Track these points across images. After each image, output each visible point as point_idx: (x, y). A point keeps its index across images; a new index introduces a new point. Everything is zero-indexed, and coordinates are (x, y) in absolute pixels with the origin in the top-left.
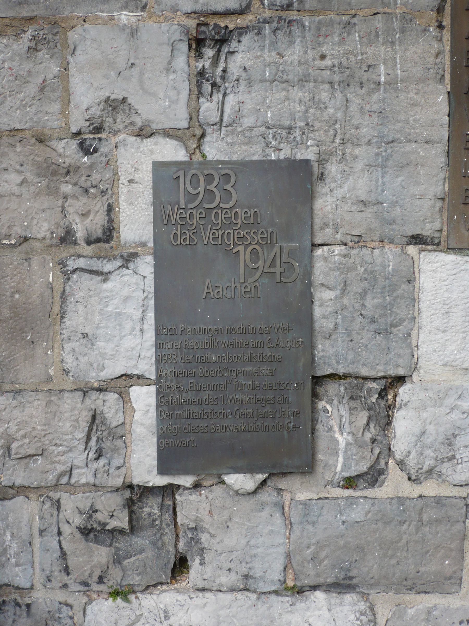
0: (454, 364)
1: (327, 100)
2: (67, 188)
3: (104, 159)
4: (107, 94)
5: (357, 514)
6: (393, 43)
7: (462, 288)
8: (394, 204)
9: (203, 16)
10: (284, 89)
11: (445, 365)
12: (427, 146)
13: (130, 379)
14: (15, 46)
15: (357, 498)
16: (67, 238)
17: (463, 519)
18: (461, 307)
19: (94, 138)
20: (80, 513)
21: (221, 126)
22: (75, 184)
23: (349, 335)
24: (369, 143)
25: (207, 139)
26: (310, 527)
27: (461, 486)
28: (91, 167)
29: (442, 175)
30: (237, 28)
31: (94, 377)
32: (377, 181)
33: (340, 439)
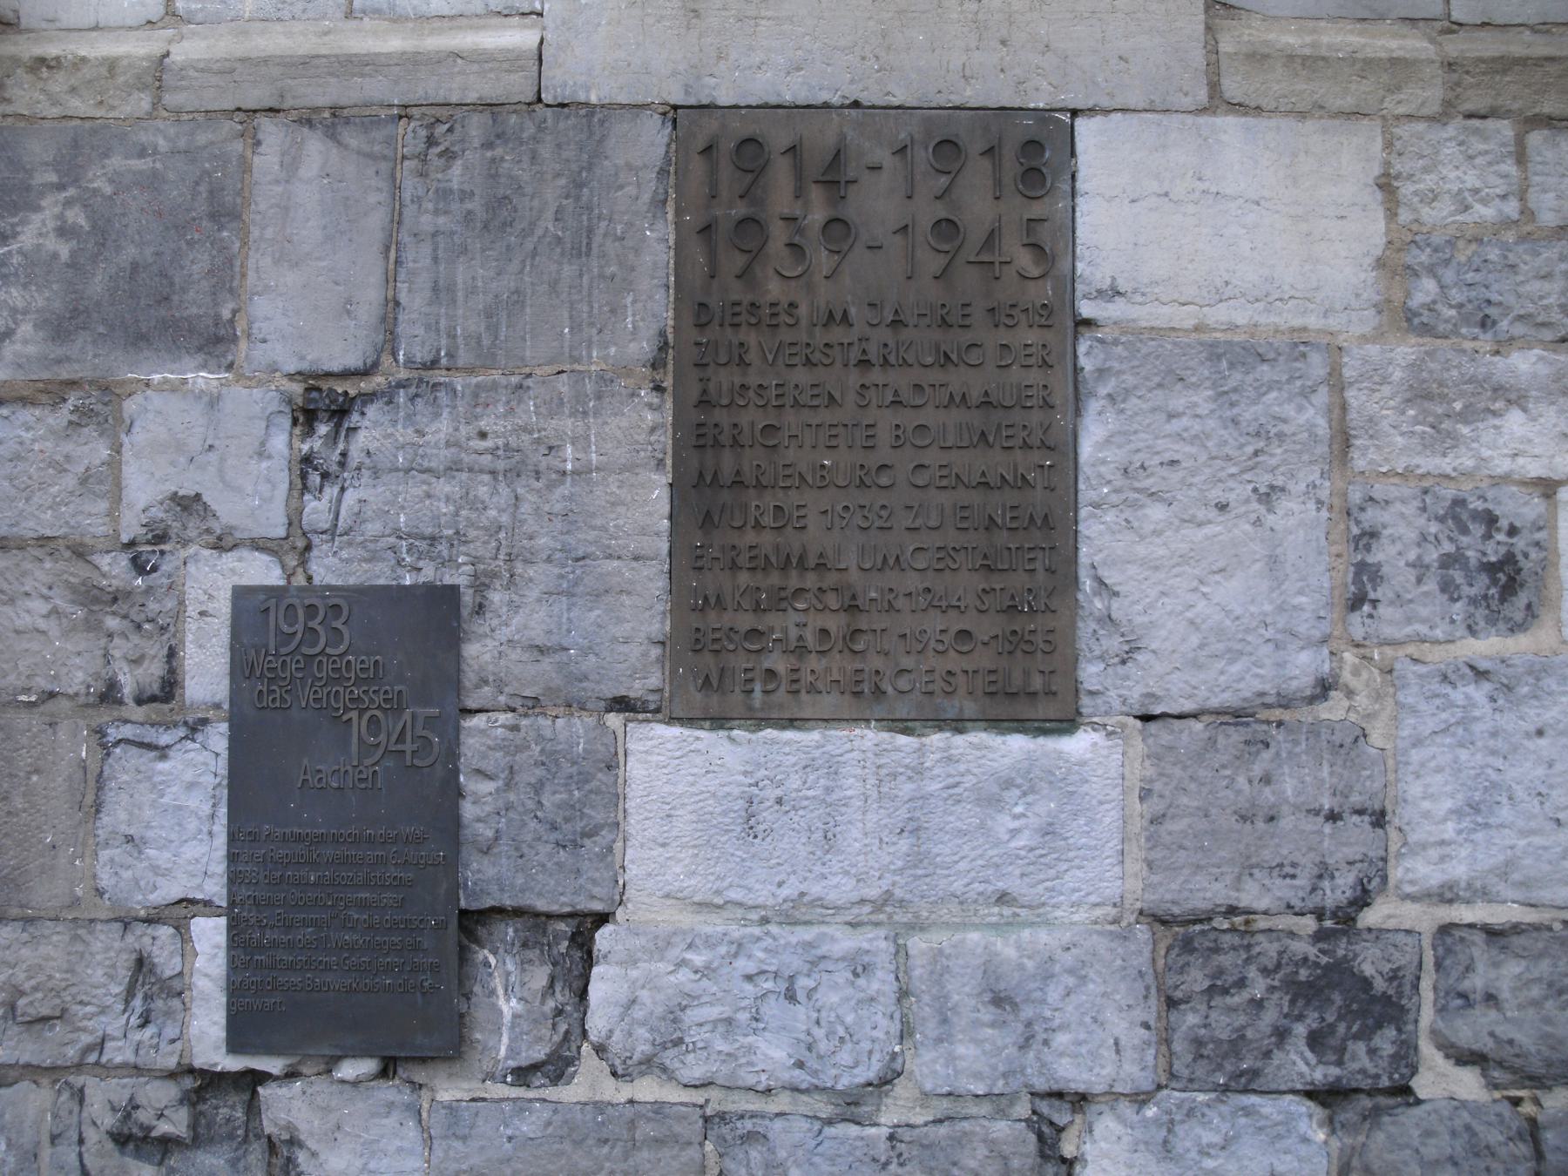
0: (680, 895)
1: (486, 497)
2: (112, 623)
3: (165, 581)
4: (173, 489)
5: (528, 1126)
6: (585, 413)
7: (691, 779)
8: (585, 652)
9: (313, 380)
10: (424, 482)
11: (667, 896)
12: (634, 564)
13: (190, 905)
14: (51, 421)
15: (530, 1100)
16: (109, 695)
17: (701, 1138)
18: (689, 808)
19: (154, 552)
20: (114, 1109)
21: (333, 535)
22: (125, 617)
23: (517, 849)
24: (549, 560)
25: (315, 553)
26: (457, 1144)
27: (695, 1087)
28: (149, 590)
29: (660, 607)
30: (360, 395)
31: (140, 902)
32: (560, 617)
33: (505, 1008)
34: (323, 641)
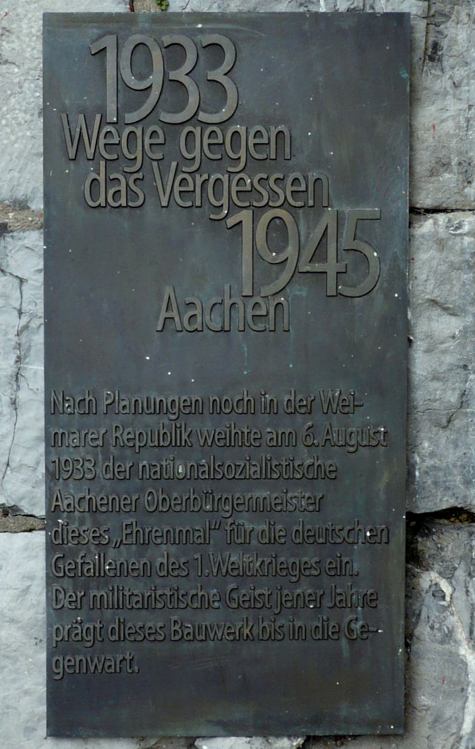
34: (193, 100)
